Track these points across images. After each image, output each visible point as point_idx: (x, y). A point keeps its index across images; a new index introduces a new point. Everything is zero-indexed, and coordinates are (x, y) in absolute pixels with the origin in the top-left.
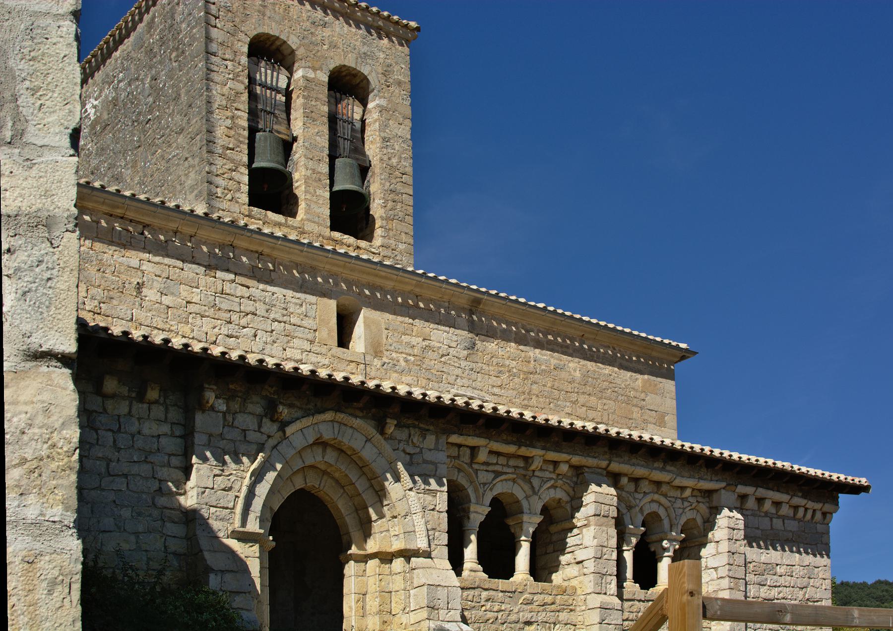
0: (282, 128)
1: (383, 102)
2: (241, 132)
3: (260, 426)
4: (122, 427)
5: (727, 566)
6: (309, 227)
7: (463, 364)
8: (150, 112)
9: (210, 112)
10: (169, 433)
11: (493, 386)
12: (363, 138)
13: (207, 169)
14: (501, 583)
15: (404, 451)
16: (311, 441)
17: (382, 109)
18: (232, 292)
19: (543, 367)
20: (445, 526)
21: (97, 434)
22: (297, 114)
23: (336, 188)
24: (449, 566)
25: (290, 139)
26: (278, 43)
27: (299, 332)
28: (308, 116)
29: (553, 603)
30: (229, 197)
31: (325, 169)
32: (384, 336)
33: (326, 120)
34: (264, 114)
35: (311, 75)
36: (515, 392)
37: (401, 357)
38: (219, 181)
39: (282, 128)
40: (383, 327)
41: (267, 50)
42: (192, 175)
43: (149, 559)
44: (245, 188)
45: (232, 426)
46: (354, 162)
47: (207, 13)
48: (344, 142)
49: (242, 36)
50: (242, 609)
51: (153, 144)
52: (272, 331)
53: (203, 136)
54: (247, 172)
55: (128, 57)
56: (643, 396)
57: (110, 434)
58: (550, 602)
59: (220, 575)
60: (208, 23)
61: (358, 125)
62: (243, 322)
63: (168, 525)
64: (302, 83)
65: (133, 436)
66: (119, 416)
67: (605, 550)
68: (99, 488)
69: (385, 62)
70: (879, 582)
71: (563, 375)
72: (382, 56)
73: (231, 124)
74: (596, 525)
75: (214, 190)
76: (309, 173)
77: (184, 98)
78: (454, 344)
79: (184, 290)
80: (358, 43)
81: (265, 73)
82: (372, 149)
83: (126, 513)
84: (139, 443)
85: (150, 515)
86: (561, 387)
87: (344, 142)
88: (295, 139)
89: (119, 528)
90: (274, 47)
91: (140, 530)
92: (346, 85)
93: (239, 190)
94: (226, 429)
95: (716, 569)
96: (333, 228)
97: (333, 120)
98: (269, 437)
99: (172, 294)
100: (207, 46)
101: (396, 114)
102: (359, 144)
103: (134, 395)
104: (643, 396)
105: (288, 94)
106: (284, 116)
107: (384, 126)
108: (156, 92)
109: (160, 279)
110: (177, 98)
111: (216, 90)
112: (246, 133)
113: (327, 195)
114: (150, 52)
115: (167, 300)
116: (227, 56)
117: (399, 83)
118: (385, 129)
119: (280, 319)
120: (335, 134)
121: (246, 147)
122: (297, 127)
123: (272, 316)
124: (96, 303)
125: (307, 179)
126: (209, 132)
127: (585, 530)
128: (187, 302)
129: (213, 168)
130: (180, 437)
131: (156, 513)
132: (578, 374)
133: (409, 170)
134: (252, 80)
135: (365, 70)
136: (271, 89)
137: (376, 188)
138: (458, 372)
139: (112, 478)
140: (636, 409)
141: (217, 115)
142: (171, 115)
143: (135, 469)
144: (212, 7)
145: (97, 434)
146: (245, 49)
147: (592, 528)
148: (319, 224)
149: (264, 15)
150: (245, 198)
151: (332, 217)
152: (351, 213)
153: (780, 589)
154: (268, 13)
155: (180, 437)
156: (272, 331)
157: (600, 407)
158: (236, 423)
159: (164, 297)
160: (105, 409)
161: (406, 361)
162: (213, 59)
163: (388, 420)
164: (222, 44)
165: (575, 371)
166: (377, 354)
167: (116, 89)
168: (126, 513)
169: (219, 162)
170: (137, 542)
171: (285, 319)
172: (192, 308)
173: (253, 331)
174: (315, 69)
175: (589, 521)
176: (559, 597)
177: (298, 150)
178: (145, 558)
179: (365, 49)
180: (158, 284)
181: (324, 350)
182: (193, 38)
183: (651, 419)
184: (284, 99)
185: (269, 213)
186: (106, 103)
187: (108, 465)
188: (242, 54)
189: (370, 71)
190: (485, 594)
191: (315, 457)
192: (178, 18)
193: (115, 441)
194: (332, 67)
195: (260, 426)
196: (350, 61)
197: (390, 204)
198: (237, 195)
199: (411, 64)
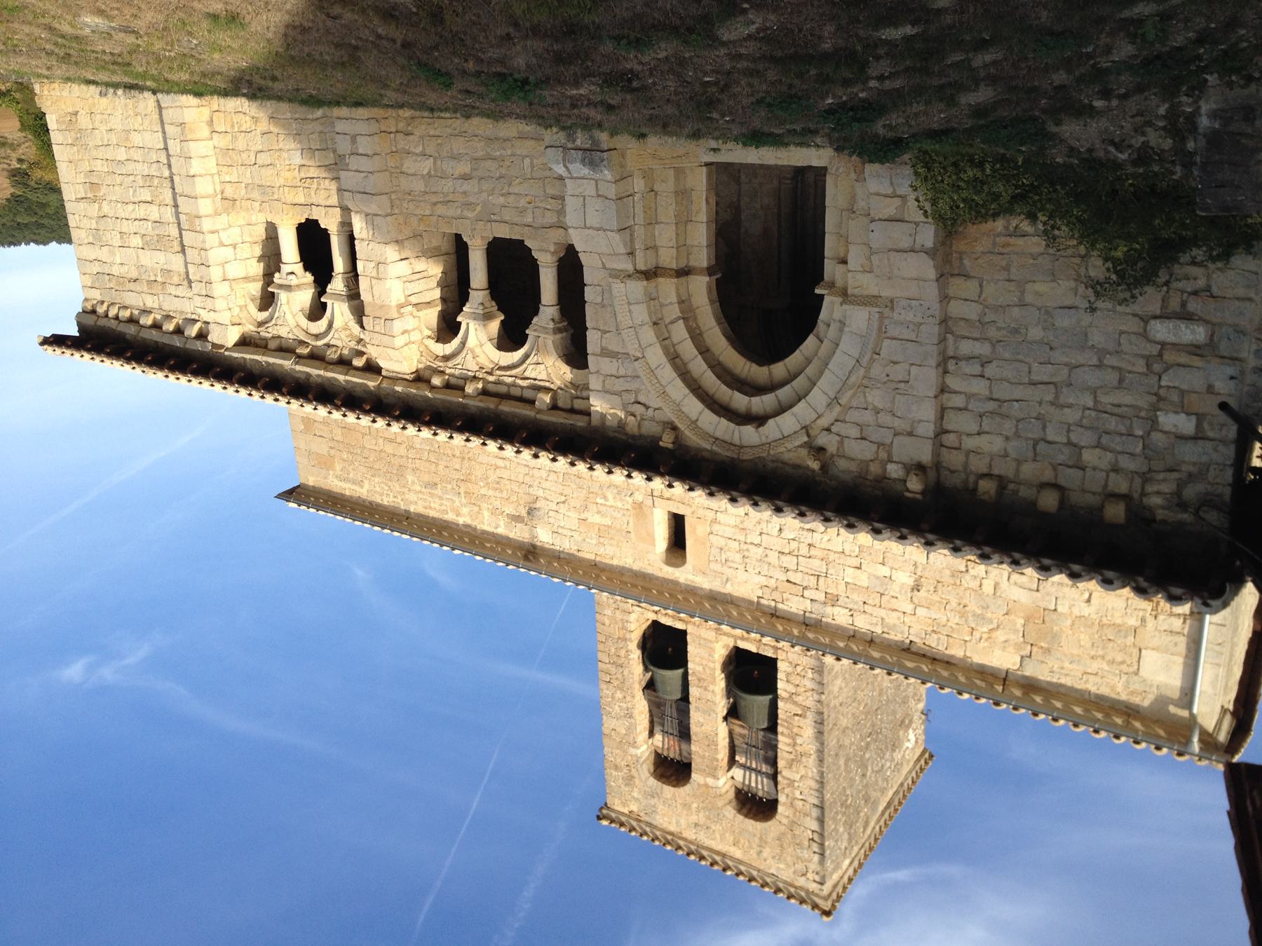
0: (738, 730)
1: (632, 751)
2: (786, 731)
3: (841, 443)
4: (1031, 447)
5: (207, 246)
6: (711, 635)
7: (540, 493)
8: (868, 744)
9: (820, 752)
10: (964, 437)
11: (505, 468)
12: (651, 715)
13: (823, 697)
14: (504, 232)
15: (647, 407)
16: (771, 422)
17: (634, 744)
18: (807, 577)
19: (449, 486)
20: (589, 311)
21: (1069, 438)
22: (723, 741)
23: (680, 671)
24: (582, 257)
25: (730, 719)
26: (745, 811)
27: (729, 532)
28: (712, 743)
29: (435, 204)
30: (799, 669)
31: (694, 691)
32: (631, 524)
33: (693, 737)
34: (763, 746)
35: (710, 781)
36: (480, 459)
37: (611, 502)
38: (810, 685)
39: (738, 730)
40: (632, 535)
41: (757, 806)
42: (836, 689)
43: (1007, 269)
44: (780, 675)
45: (880, 445)
46: (660, 694)
47: (822, 845)
48: (672, 713)
49: (785, 821)
50: (886, 196)
51: (868, 713)
52: (761, 534)
53: (826, 729)
54: (779, 692)
55: (883, 791)
56: (333, 452)
57: (1050, 438)
58: (439, 205)
59: (918, 247)
60: (822, 835)
61: (657, 729)
62: (794, 545)
63: (974, 317)
64: (720, 773)
65: (1017, 435)
66: (1034, 460)
67: (374, 274)
68: (1073, 367)
69: (636, 794)
70: (45, 243)
71: (426, 478)
72: (635, 794)
73: (796, 737)
74: (389, 307)
75: (816, 675)
76: (711, 687)
77: (842, 762)
78: (551, 514)
79: (863, 579)
80: (661, 807)
81: (760, 785)
82: (641, 707)
83: (1035, 333)
84: (1008, 427)
85: (999, 329)
86: (427, 464)
87: (672, 713)
88: (725, 719)
89: (1047, 312)
90: (748, 806)
91: (1016, 310)
92: (673, 770)
93: (788, 674)
94: (888, 441)
95: (222, 244)
96: (684, 633)
97: (684, 734)
98: (828, 430)
99: (877, 578)
100: (823, 814)
101: (618, 740)
102: (655, 711)
103: (1011, 486)
104: (333, 452)
105: (732, 762)
106: (736, 742)
107: (631, 729)
108: (863, 765)
109: (892, 593)
110: (848, 760)
111: (813, 771)
112: (780, 729)
113: (690, 665)
114: (867, 799)
115: (885, 571)
116: (801, 803)
117: (616, 768)
118: (631, 733)
119: (751, 547)
120: (680, 723)
121: (780, 716)
122: (723, 730)
123: (760, 550)
124: (972, 572)
125: (714, 682)
126: (820, 733)
127: (403, 300)
128: (859, 568)
129: (816, 697)
130: (947, 432)
131: (992, 333)
132: (410, 478)
133: (603, 686)
134: (774, 777)
135: (653, 782)
136: (750, 769)
137: (636, 670)
138: (545, 485)
139: (1054, 380)
140: (339, 438)
141: (812, 748)
142: (852, 744)
143: (1018, 392)
144: (816, 850)
145: (1069, 438)
146: (780, 809)
147: (394, 303)
148: (700, 637)
149: (761, 838)
150: (780, 665)
151: (685, 643)
152: (664, 648)
153: (133, 216)
154: (757, 840)
155: (947, 432)
156: (761, 534)
157: (381, 441)
158: (874, 447)
159: (888, 574)
160: (1055, 470)
161: (605, 498)
162: (816, 801)
163: (670, 446)
164: (806, 815)
165: (413, 483)
166: (639, 506)
167: (893, 760)
168: (1035, 333)
169: (810, 702)
170: (1023, 292)
171: (745, 547)
172: (856, 562)
173: (783, 535)
174: (706, 786)
175: (398, 312)
176: (428, 212)
177: (722, 706)
178: (1013, 270)
179: (652, 802)
180: (894, 589)
181: (701, 512)
182: (834, 819)
183: (321, 426)
184: (737, 758)
185: (754, 650)
186: (900, 746)
187: (1057, 397)
188: (784, 804)
189: (645, 778)
190: (529, 220)
191: (759, 404)
192: (846, 836)
193: (1044, 428)
194: (687, 788)
195: (841, 443)
196: (668, 791)
197: (623, 653)
198: (790, 670)
199: (605, 786)
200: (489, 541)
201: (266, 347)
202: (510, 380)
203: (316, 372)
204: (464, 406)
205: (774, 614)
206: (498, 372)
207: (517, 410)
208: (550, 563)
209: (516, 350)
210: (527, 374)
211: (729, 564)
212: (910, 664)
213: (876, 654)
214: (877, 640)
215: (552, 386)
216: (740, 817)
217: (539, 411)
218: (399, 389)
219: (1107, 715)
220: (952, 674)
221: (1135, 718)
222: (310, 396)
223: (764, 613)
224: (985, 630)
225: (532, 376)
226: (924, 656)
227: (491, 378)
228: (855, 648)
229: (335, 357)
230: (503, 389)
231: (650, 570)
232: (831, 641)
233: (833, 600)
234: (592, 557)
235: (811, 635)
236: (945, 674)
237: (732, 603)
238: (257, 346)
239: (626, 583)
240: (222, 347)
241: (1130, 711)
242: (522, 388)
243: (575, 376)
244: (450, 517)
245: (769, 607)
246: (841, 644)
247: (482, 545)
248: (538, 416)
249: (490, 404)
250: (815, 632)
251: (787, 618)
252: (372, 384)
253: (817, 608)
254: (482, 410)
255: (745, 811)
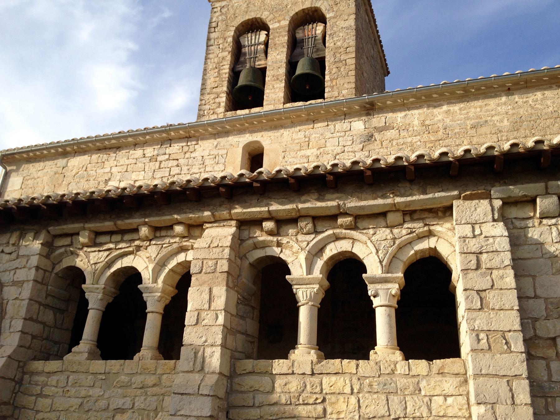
26: (254, 20)
30: (212, 112)
200: (412, 103)
201: (405, 213)
202: (120, 246)
203: (311, 204)
204: (145, 216)
205: (188, 138)
206: (131, 249)
207: (98, 225)
208: (350, 108)
209: (152, 270)
210: (106, 253)
211: (213, 156)
212: (113, 141)
213: (130, 139)
214: (132, 147)
215: (85, 249)
216: (258, 16)
217: (84, 229)
218: (207, 213)
219: (35, 155)
220: (95, 145)
221: (27, 158)
222: (369, 173)
223: (194, 136)
224: (80, 173)
225: (102, 253)
226: (110, 149)
227: (137, 243)
228: (141, 138)
229: (302, 224)
230: (127, 237)
231: (271, 133)
232: (153, 137)
233: (153, 159)
234: (316, 125)
235: (164, 135)
236: (98, 144)
237: (215, 135)
238: (430, 211)
239: (286, 118)
240: (466, 198)
241: (29, 160)
242: (111, 242)
243: (74, 260)
244: (456, 108)
245: (191, 141)
246: (148, 137)
247: (418, 98)
248: (82, 225)
249: (123, 224)
250: (163, 138)
251: (180, 139)
252: (238, 210)
253: (162, 151)
254: (131, 217)
255: (254, 20)
